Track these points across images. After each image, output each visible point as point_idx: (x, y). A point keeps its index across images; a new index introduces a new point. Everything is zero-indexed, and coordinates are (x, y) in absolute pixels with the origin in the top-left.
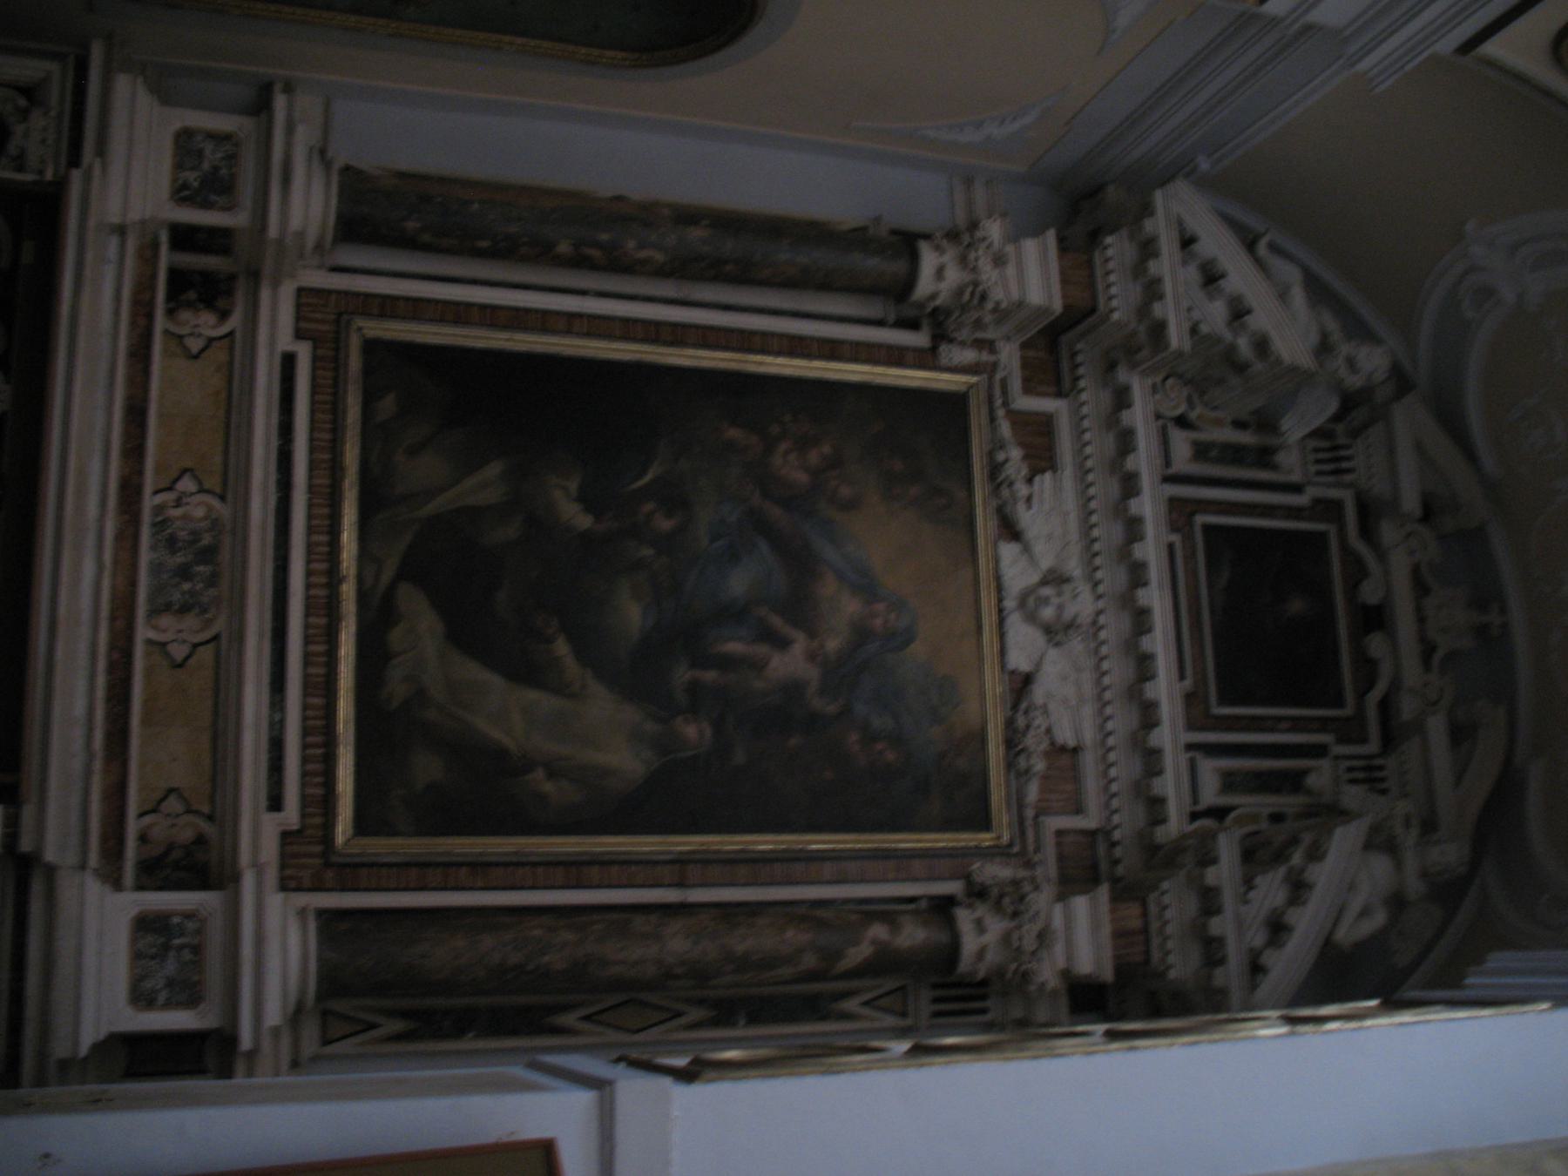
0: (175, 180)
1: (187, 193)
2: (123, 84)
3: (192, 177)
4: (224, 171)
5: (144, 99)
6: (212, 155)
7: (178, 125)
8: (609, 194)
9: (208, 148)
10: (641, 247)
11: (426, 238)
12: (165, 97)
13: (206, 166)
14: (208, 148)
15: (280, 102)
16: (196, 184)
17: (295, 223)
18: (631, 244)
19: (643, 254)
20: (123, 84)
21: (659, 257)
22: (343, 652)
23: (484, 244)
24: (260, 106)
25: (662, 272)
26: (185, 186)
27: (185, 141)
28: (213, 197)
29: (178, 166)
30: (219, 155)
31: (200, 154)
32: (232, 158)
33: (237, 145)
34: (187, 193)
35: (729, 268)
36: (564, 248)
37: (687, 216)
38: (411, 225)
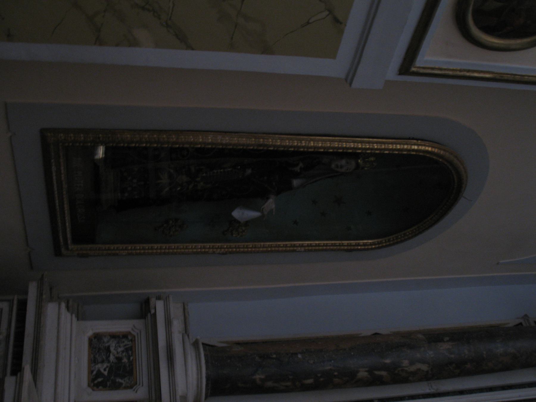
0: (91, 372)
1: (100, 380)
2: (51, 310)
3: (102, 367)
4: (125, 360)
5: (66, 316)
6: (116, 350)
7: (90, 333)
8: (369, 334)
9: (113, 344)
10: (412, 363)
11: (270, 384)
12: (81, 317)
13: (112, 358)
14: (113, 344)
15: (160, 306)
16: (106, 373)
17: (180, 389)
18: (406, 363)
19: (413, 368)
20: (51, 310)
21: (424, 367)
22: (67, 218)
23: (310, 381)
24: (145, 310)
25: (427, 377)
26: (99, 374)
27: (96, 343)
28: (119, 380)
29: (93, 361)
30: (120, 350)
31: (108, 350)
32: (130, 350)
33: (133, 340)
34: (100, 380)
35: (468, 366)
36: (363, 374)
37: (435, 337)
38: (258, 377)
